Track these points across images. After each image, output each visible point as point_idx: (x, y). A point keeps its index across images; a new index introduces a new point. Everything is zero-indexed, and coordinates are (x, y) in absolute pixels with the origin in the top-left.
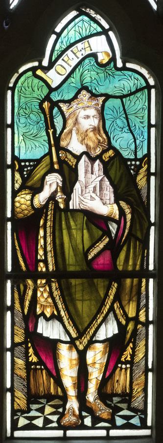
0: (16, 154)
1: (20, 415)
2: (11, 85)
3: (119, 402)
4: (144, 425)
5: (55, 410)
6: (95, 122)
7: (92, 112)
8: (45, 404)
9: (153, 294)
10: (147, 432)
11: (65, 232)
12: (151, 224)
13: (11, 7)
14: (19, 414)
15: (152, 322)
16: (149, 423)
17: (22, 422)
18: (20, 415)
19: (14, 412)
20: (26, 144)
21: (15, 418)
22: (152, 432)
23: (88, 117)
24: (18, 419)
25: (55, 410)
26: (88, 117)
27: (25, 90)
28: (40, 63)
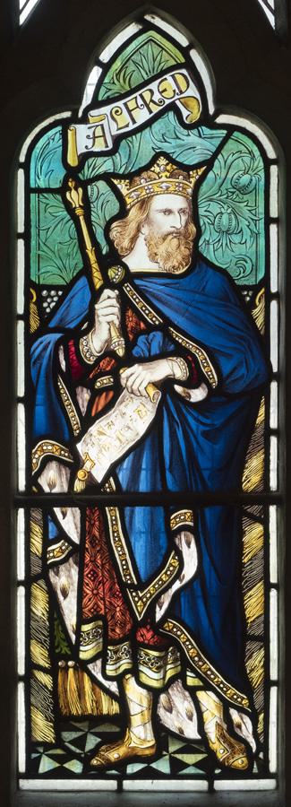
0: (33, 278)
1: (42, 751)
2: (22, 159)
3: (178, 752)
4: (264, 773)
5: (57, 765)
6: (177, 222)
7: (178, 202)
8: (42, 754)
9: (17, 453)
10: (269, 784)
11: (191, 435)
12: (272, 376)
13: (23, 18)
14: (84, 726)
15: (20, 583)
16: (273, 767)
17: (46, 764)
18: (42, 751)
19: (32, 745)
20: (46, 251)
21: (34, 755)
22: (277, 782)
23: (168, 212)
24: (38, 760)
25: (57, 765)
26: (168, 212)
27: (43, 157)
28: (75, 112)
